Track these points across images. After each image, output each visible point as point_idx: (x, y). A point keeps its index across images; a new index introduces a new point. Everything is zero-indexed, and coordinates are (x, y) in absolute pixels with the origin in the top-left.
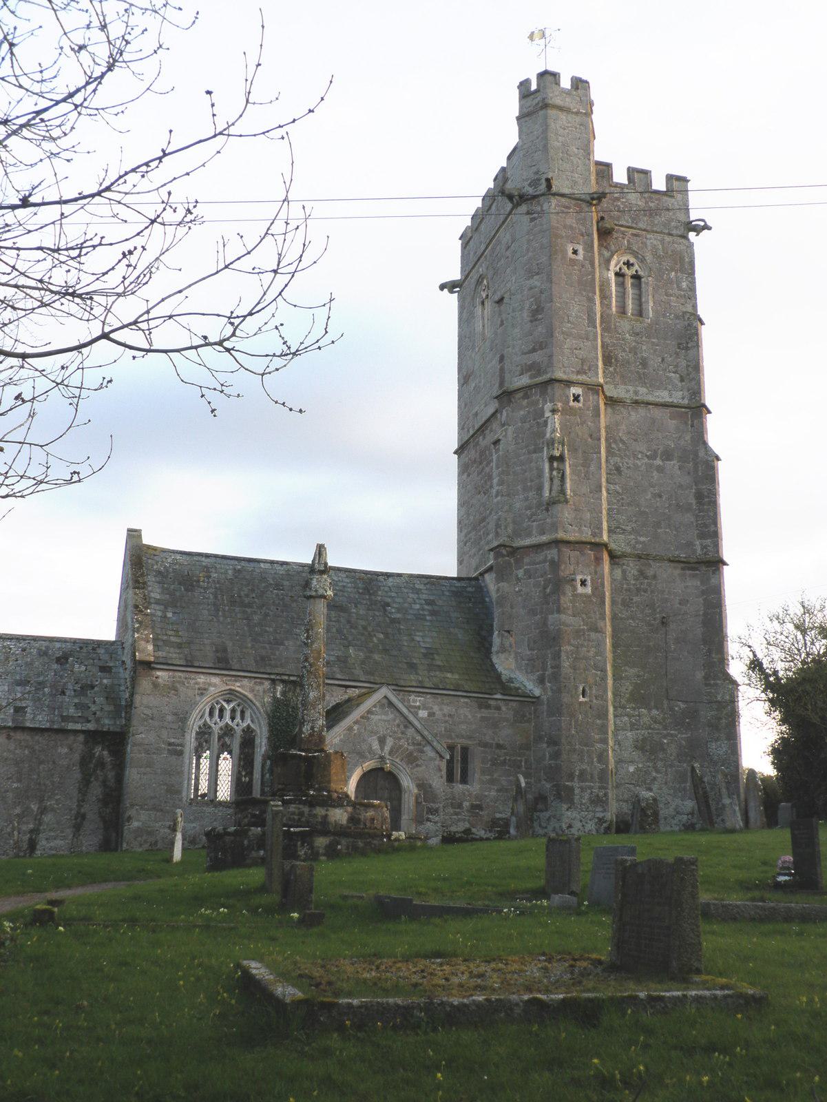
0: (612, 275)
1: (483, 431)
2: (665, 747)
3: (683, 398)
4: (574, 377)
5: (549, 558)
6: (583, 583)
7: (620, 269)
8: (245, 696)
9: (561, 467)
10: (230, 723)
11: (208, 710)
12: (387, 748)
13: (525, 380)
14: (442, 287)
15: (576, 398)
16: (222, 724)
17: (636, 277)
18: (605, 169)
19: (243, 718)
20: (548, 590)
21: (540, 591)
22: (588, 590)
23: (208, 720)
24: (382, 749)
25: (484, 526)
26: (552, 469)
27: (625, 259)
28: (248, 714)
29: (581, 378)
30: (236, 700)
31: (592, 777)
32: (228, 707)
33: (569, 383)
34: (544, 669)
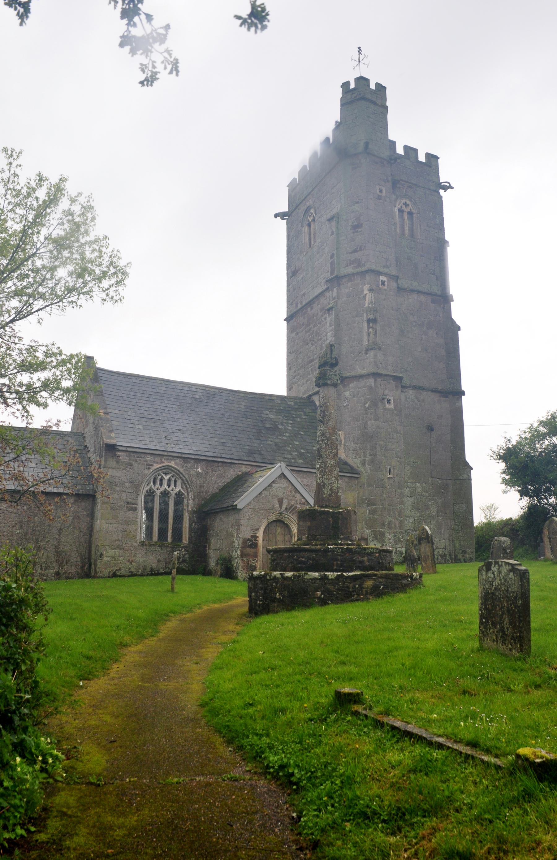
0: (396, 210)
1: (311, 305)
2: (430, 507)
3: (438, 291)
4: (382, 270)
5: (368, 384)
6: (389, 401)
7: (401, 207)
8: (179, 471)
9: (374, 326)
10: (167, 488)
11: (152, 479)
12: (284, 507)
13: (350, 270)
14: (276, 216)
15: (383, 283)
16: (162, 489)
17: (410, 214)
18: (393, 144)
19: (175, 485)
20: (367, 405)
21: (361, 407)
22: (392, 406)
23: (153, 487)
24: (281, 506)
25: (312, 365)
26: (369, 327)
27: (404, 201)
28: (179, 482)
29: (386, 270)
30: (171, 473)
31: (395, 526)
32: (166, 478)
33: (379, 273)
34: (365, 455)
